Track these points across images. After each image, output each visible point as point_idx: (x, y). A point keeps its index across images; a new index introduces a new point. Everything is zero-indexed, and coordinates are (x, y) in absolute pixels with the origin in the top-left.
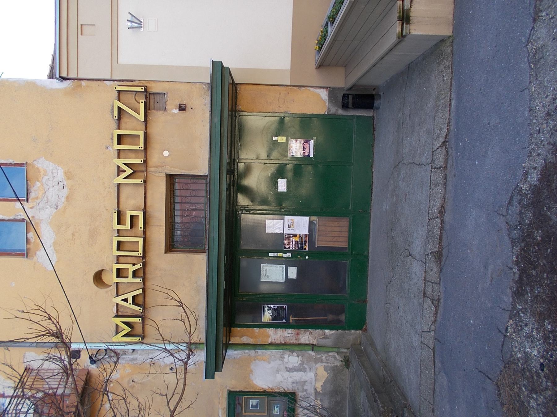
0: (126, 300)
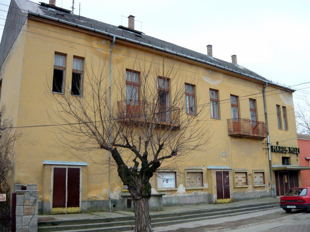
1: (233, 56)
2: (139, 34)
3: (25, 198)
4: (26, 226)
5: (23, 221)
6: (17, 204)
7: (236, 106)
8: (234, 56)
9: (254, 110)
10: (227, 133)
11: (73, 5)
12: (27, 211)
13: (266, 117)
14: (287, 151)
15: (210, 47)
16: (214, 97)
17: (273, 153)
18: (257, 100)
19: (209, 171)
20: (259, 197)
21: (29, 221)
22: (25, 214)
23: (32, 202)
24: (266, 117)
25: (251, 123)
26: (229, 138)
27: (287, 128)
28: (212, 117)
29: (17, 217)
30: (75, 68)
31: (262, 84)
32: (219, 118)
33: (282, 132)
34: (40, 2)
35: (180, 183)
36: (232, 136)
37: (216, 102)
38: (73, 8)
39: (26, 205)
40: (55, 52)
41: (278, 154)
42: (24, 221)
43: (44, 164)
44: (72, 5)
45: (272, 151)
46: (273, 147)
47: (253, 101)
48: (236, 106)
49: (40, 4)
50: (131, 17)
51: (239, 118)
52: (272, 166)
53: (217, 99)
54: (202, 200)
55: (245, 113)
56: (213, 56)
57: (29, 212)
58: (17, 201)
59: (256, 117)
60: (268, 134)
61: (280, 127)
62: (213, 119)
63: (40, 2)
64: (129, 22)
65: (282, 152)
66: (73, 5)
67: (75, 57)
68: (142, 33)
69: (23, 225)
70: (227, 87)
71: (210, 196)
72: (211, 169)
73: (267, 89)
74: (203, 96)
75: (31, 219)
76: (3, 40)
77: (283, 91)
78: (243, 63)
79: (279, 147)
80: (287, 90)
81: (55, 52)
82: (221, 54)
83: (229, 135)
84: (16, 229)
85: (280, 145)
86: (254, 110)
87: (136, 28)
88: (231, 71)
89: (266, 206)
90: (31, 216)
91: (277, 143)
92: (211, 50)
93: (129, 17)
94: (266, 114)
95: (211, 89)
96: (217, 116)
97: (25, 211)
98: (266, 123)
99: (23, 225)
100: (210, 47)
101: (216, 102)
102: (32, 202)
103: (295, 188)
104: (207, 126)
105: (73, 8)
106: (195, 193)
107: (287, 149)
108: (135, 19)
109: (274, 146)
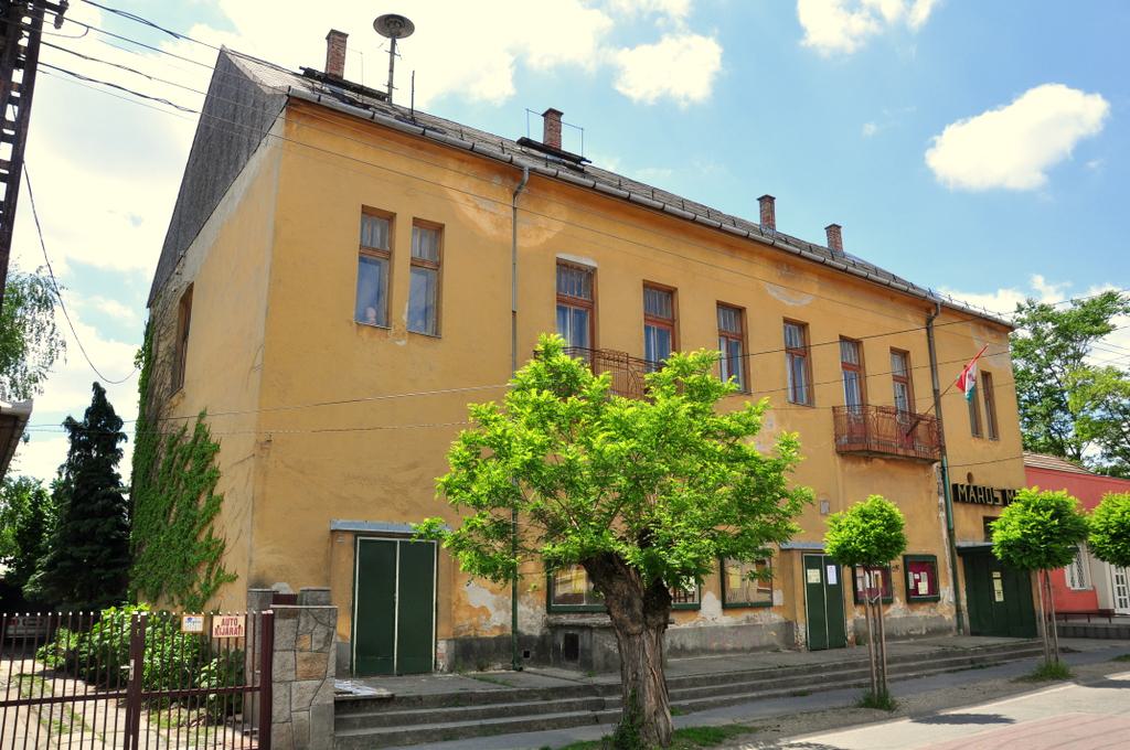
1: (830, 227)
2: (575, 163)
3: (300, 628)
4: (301, 710)
5: (293, 698)
6: (275, 647)
7: (855, 370)
8: (833, 229)
9: (904, 381)
10: (831, 447)
11: (391, 77)
12: (306, 667)
13: (937, 404)
14: (996, 499)
15: (767, 201)
16: (735, 329)
17: (958, 505)
18: (912, 354)
19: (787, 555)
20: (924, 632)
21: (310, 696)
22: (299, 675)
23: (318, 642)
24: (937, 404)
25: (898, 418)
26: (838, 460)
27: (994, 435)
28: (791, 399)
29: (275, 686)
30: (417, 255)
31: (929, 308)
32: (810, 403)
33: (981, 447)
34: (301, 68)
35: (707, 589)
36: (845, 453)
37: (799, 354)
38: (390, 85)
39: (301, 651)
40: (414, 218)
41: (972, 509)
42: (295, 696)
43: (333, 531)
44: (387, 79)
45: (956, 499)
46: (959, 488)
47: (903, 355)
48: (855, 370)
49: (302, 72)
50: (552, 116)
51: (864, 405)
52: (957, 544)
53: (739, 332)
54: (772, 637)
55: (881, 392)
56: (779, 228)
57: (310, 672)
58: (276, 638)
59: (911, 401)
60: (942, 449)
61: (976, 431)
62: (793, 406)
63: (301, 68)
64: (545, 128)
65: (983, 503)
66: (391, 77)
67: (417, 222)
68: (584, 160)
69: (294, 707)
70: (831, 315)
71: (789, 626)
72: (793, 549)
73: (944, 328)
74: (766, 339)
75: (316, 691)
76: (189, 171)
77: (982, 328)
78: (857, 247)
79: (975, 488)
80: (993, 324)
81: (414, 218)
82: (801, 224)
83: (838, 452)
84: (273, 720)
85: (979, 482)
86: (904, 381)
87: (568, 145)
88: (861, 277)
89: (919, 663)
90: (318, 683)
91: (970, 476)
92: (772, 211)
93: (544, 115)
94: (936, 392)
95: (786, 321)
96: (802, 394)
97: (299, 667)
98: (939, 420)
99: (294, 707)
100: (767, 201)
101: (799, 354)
102: (318, 642)
103: (398, 540)
104: (1010, 461)
105: (390, 85)
106: (748, 620)
107: (998, 495)
108: (562, 119)
109: (962, 486)
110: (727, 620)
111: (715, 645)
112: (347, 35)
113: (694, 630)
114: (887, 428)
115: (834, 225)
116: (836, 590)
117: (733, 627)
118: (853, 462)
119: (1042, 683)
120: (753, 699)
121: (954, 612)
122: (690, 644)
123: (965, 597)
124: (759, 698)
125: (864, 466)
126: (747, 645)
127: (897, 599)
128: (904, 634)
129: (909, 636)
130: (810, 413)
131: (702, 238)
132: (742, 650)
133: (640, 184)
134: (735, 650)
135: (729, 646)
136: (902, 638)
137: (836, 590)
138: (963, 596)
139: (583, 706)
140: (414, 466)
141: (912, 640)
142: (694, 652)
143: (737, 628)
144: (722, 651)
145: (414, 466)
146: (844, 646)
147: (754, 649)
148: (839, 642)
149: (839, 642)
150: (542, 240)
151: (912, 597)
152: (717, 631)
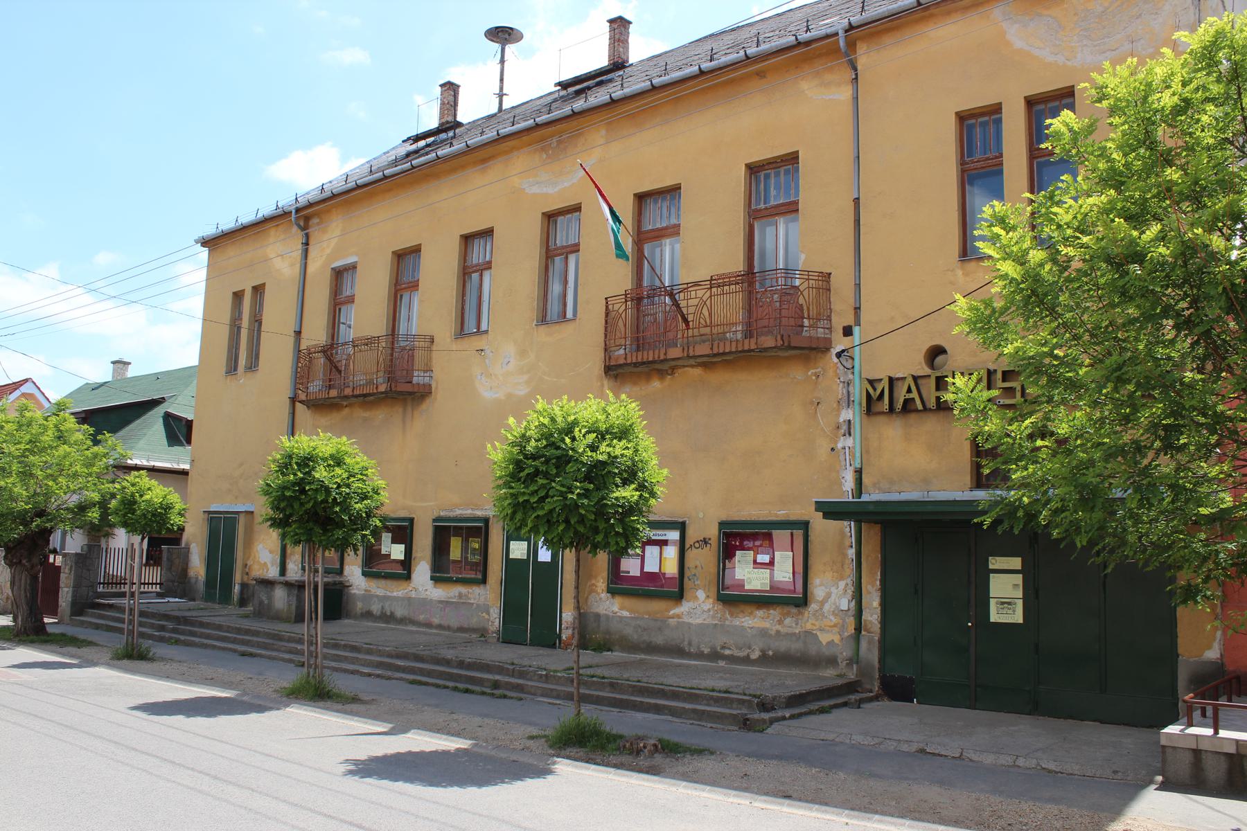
0: (909, 391)
20: (755, 655)
106: (460, 596)
110: (438, 593)
111: (422, 618)
112: (630, 23)
113: (403, 599)
114: (365, 370)
115: (621, 18)
116: (551, 570)
117: (441, 602)
118: (635, 383)
119: (581, 752)
120: (283, 660)
121: (851, 630)
122: (399, 613)
123: (876, 603)
124: (224, 649)
125: (656, 384)
126: (454, 623)
127: (701, 594)
128: (706, 651)
129: (715, 656)
130: (567, 330)
131: (453, 170)
132: (448, 628)
133: (666, 53)
134: (440, 627)
135: (436, 621)
136: (700, 656)
137: (551, 570)
138: (873, 602)
139: (152, 626)
140: (241, 464)
141: (722, 663)
142: (402, 621)
143: (446, 603)
144: (429, 625)
145: (241, 464)
146: (553, 646)
147: (461, 629)
148: (547, 638)
149: (547, 638)
150: (1051, 59)
151: (441, 572)
152: (425, 603)
